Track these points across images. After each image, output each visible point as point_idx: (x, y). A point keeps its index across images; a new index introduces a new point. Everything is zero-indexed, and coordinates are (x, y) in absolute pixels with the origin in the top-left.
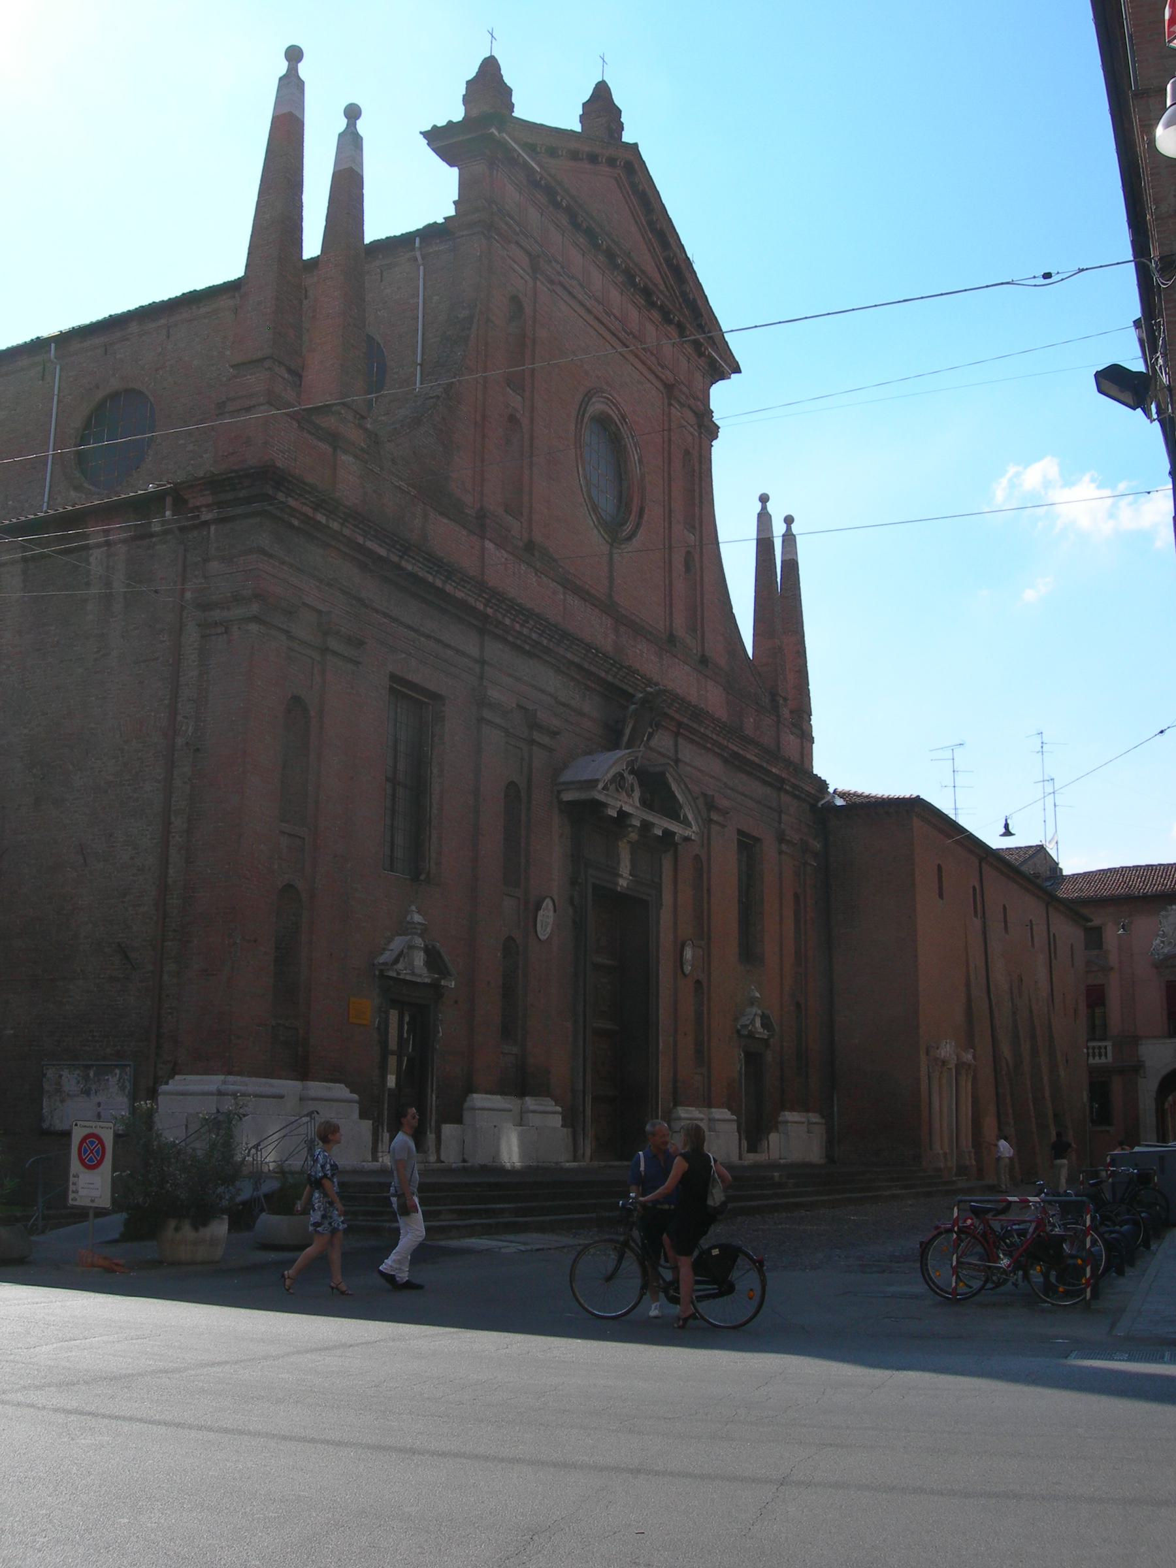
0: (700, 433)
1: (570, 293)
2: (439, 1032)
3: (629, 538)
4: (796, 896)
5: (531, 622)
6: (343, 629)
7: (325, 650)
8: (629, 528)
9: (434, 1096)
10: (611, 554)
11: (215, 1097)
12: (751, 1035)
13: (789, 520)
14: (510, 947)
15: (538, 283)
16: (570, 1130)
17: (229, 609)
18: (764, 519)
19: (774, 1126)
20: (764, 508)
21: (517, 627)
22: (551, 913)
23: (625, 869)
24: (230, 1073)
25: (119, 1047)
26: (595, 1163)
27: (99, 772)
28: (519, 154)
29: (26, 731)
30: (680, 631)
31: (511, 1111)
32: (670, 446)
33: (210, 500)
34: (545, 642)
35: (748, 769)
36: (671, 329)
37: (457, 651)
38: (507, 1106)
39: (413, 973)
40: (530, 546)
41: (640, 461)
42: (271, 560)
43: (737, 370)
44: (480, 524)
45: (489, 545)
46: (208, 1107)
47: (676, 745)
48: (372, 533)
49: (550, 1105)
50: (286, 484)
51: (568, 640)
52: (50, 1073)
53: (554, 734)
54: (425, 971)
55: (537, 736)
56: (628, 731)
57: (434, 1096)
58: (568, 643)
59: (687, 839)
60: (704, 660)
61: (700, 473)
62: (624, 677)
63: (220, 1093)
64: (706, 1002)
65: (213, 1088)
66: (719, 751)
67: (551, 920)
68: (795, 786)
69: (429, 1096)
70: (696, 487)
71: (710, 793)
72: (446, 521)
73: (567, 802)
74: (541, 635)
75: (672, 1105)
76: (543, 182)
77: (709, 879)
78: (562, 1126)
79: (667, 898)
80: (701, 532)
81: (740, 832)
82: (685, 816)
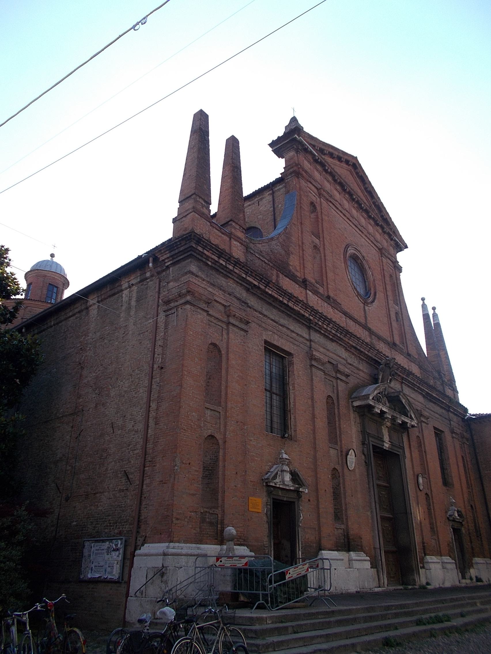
0: (395, 269)
1: (335, 206)
2: (301, 517)
3: (373, 302)
4: (462, 457)
5: (331, 325)
6: (237, 314)
7: (228, 323)
8: (371, 299)
9: (300, 552)
10: (364, 307)
11: (162, 557)
12: (454, 520)
13: (434, 309)
14: (335, 474)
15: (322, 199)
16: (375, 569)
17: (177, 301)
18: (424, 306)
19: (471, 565)
20: (424, 302)
21: (325, 326)
22: (354, 457)
23: (386, 438)
24: (171, 541)
25: (121, 529)
26: (392, 588)
27: (122, 387)
28: (308, 147)
29: (94, 374)
30: (398, 343)
31: (343, 560)
32: (383, 271)
33: (168, 255)
34: (339, 335)
35: (434, 401)
36: (378, 228)
37: (298, 334)
38: (341, 558)
39: (284, 484)
40: (328, 297)
41: (373, 275)
42: (196, 278)
43: (406, 247)
44: (304, 283)
45: (308, 291)
46: (158, 562)
47: (402, 388)
48: (250, 273)
49: (363, 556)
50: (202, 243)
51: (349, 335)
52: (87, 544)
53: (347, 376)
54: (291, 483)
55: (339, 376)
56: (380, 377)
57: (300, 552)
58: (349, 336)
59: (413, 426)
60: (409, 355)
61: (397, 284)
62: (376, 355)
63: (165, 554)
64: (431, 504)
65: (161, 551)
66: (420, 392)
67: (354, 461)
68: (455, 410)
69: (298, 552)
70: (396, 289)
71: (419, 409)
72: (288, 279)
73: (356, 406)
74: (336, 332)
75: (423, 555)
76: (319, 160)
77: (425, 447)
78: (371, 568)
79: (407, 454)
80: (401, 305)
81: (435, 428)
82: (411, 416)
